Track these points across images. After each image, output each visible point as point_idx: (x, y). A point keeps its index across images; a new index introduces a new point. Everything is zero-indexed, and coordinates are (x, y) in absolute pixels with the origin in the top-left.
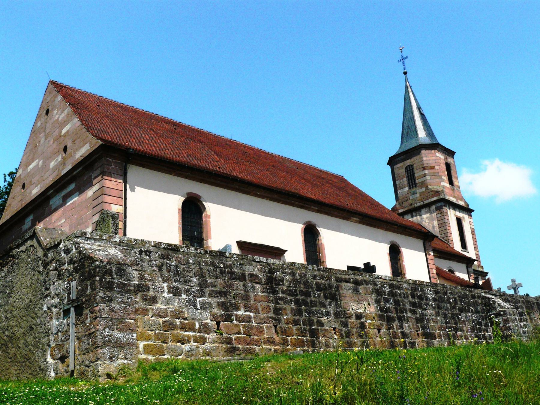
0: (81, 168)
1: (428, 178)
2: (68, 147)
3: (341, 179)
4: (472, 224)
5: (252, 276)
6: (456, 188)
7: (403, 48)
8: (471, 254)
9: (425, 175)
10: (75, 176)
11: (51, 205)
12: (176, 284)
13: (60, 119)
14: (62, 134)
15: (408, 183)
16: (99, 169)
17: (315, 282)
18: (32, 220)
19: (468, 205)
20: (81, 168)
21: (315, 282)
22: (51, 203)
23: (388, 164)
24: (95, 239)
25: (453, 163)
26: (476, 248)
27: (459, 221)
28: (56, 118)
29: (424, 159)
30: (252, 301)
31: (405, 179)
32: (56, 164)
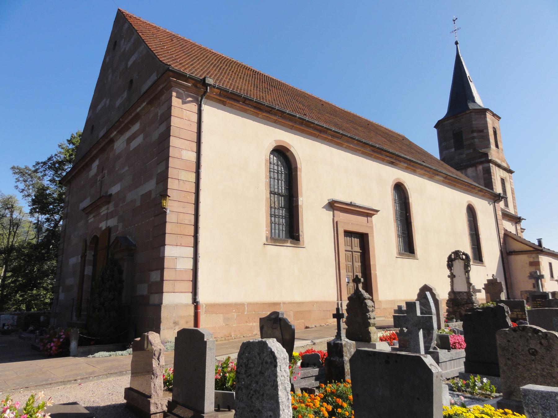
0: (145, 103)
1: (476, 140)
3: (404, 139)
6: (500, 151)
7: (457, 19)
9: (474, 138)
10: (138, 114)
11: (116, 149)
13: (127, 49)
14: (129, 66)
18: (98, 166)
20: (145, 103)
22: (115, 147)
25: (498, 127)
26: (515, 207)
27: (503, 181)
28: (122, 50)
29: (473, 122)
31: (452, 141)
32: (122, 101)
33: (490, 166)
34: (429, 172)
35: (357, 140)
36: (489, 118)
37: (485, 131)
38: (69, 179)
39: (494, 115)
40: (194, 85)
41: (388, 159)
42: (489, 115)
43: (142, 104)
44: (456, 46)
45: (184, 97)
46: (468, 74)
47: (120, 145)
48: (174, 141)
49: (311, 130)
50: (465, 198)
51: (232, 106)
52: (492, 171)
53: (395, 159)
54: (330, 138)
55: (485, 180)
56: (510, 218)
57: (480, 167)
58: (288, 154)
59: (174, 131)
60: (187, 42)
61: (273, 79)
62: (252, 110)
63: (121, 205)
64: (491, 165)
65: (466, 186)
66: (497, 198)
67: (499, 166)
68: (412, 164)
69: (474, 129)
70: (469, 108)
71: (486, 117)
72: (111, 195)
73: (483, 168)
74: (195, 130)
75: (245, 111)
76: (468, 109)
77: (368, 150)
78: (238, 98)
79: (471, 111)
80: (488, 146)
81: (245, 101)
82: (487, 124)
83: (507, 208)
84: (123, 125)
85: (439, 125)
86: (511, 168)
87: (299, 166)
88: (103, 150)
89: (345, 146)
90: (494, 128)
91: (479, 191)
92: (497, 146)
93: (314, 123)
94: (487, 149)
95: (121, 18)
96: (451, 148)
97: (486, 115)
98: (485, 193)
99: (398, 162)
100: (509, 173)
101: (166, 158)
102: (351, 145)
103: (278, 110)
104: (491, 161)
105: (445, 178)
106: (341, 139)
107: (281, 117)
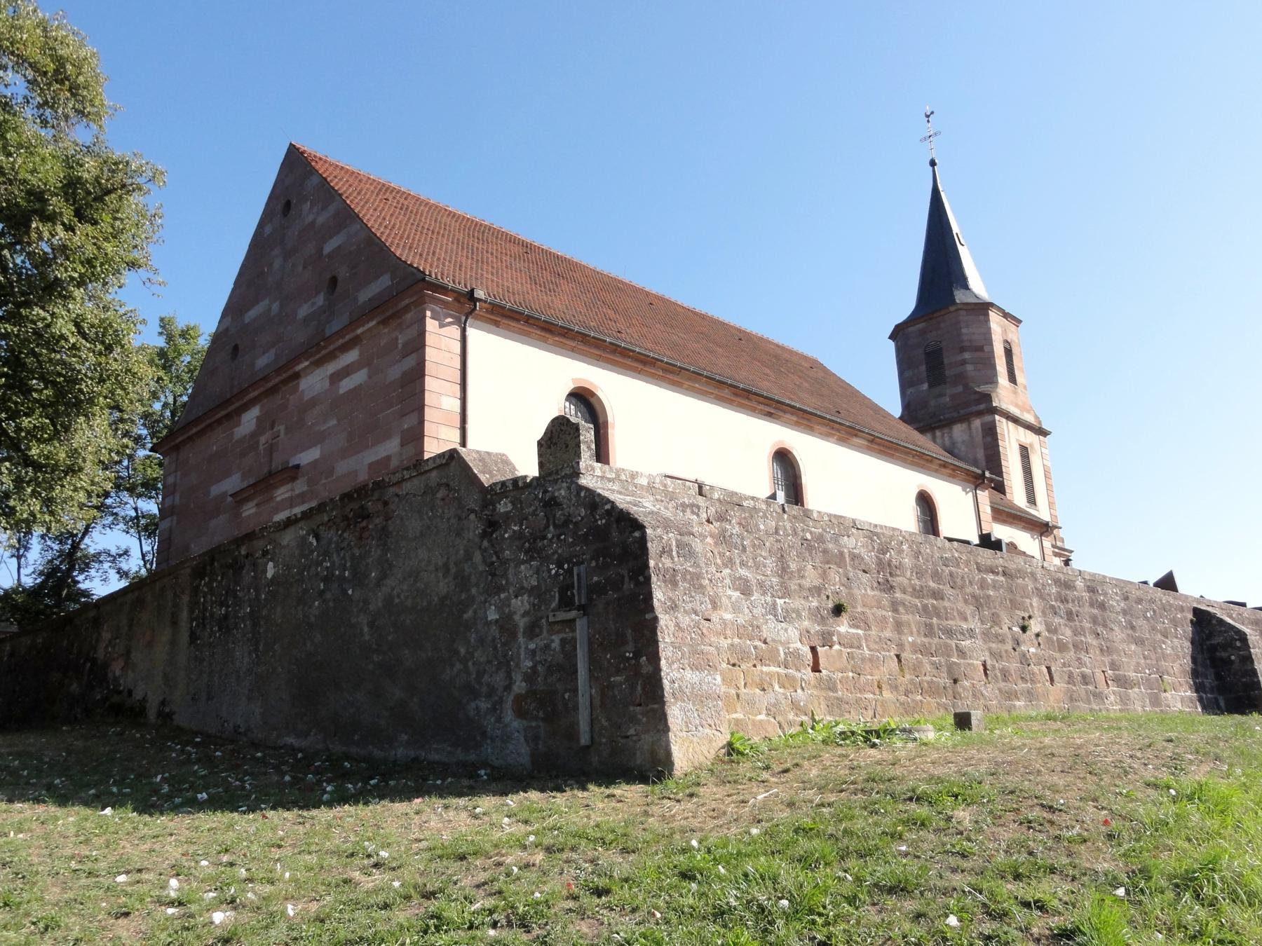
0: (374, 323)
1: (969, 367)
2: (340, 279)
3: (814, 365)
4: (1047, 457)
5: (854, 557)
6: (1020, 389)
7: (932, 113)
8: (1043, 513)
9: (964, 362)
12: (743, 572)
15: (928, 376)
16: (416, 325)
17: (947, 570)
19: (1040, 422)
20: (374, 323)
21: (947, 570)
23: (890, 338)
24: (609, 480)
26: (1051, 505)
27: (1025, 452)
29: (964, 331)
30: (859, 607)
31: (923, 368)
33: (994, 421)
34: (838, 430)
35: (706, 377)
36: (996, 323)
37: (986, 349)
38: (177, 441)
39: (1006, 315)
40: (457, 300)
41: (761, 407)
42: (994, 317)
43: (368, 323)
44: (931, 168)
45: (442, 317)
46: (955, 228)
47: (314, 382)
48: (430, 383)
49: (628, 362)
50: (917, 480)
51: (508, 328)
52: (998, 431)
53: (775, 408)
54: (661, 373)
55: (985, 449)
56: (1026, 523)
57: (977, 423)
58: (593, 400)
59: (429, 368)
60: (407, 196)
61: (558, 256)
62: (539, 333)
63: (324, 481)
64: (997, 417)
65: (913, 457)
66: (980, 481)
67: (1016, 420)
68: (806, 416)
69: (966, 344)
70: (955, 300)
71: (987, 321)
72: (297, 467)
73: (982, 425)
74: (458, 366)
75: (527, 334)
76: (953, 302)
77: (726, 392)
78: (518, 316)
79: (959, 307)
80: (992, 379)
81: (528, 319)
82: (991, 334)
83: (1033, 506)
84: (323, 352)
85: (898, 334)
86: (1045, 426)
87: (610, 419)
88: (274, 390)
89: (685, 386)
90: (1006, 341)
91: (941, 465)
92: (1012, 378)
93: (634, 351)
94: (990, 386)
95: (296, 162)
96: (922, 383)
97: (988, 315)
98: (954, 470)
99: (781, 414)
100: (1039, 434)
101: (420, 408)
102: (697, 385)
103: (577, 332)
104: (995, 411)
105: (872, 441)
106: (678, 374)
107: (582, 341)
